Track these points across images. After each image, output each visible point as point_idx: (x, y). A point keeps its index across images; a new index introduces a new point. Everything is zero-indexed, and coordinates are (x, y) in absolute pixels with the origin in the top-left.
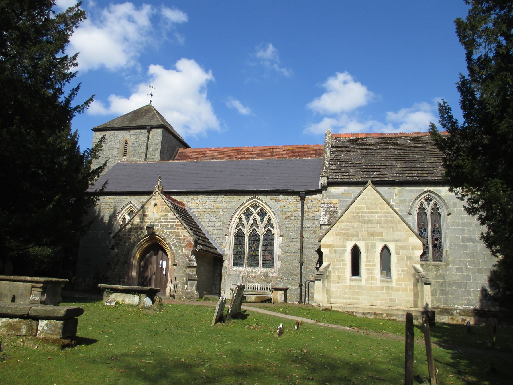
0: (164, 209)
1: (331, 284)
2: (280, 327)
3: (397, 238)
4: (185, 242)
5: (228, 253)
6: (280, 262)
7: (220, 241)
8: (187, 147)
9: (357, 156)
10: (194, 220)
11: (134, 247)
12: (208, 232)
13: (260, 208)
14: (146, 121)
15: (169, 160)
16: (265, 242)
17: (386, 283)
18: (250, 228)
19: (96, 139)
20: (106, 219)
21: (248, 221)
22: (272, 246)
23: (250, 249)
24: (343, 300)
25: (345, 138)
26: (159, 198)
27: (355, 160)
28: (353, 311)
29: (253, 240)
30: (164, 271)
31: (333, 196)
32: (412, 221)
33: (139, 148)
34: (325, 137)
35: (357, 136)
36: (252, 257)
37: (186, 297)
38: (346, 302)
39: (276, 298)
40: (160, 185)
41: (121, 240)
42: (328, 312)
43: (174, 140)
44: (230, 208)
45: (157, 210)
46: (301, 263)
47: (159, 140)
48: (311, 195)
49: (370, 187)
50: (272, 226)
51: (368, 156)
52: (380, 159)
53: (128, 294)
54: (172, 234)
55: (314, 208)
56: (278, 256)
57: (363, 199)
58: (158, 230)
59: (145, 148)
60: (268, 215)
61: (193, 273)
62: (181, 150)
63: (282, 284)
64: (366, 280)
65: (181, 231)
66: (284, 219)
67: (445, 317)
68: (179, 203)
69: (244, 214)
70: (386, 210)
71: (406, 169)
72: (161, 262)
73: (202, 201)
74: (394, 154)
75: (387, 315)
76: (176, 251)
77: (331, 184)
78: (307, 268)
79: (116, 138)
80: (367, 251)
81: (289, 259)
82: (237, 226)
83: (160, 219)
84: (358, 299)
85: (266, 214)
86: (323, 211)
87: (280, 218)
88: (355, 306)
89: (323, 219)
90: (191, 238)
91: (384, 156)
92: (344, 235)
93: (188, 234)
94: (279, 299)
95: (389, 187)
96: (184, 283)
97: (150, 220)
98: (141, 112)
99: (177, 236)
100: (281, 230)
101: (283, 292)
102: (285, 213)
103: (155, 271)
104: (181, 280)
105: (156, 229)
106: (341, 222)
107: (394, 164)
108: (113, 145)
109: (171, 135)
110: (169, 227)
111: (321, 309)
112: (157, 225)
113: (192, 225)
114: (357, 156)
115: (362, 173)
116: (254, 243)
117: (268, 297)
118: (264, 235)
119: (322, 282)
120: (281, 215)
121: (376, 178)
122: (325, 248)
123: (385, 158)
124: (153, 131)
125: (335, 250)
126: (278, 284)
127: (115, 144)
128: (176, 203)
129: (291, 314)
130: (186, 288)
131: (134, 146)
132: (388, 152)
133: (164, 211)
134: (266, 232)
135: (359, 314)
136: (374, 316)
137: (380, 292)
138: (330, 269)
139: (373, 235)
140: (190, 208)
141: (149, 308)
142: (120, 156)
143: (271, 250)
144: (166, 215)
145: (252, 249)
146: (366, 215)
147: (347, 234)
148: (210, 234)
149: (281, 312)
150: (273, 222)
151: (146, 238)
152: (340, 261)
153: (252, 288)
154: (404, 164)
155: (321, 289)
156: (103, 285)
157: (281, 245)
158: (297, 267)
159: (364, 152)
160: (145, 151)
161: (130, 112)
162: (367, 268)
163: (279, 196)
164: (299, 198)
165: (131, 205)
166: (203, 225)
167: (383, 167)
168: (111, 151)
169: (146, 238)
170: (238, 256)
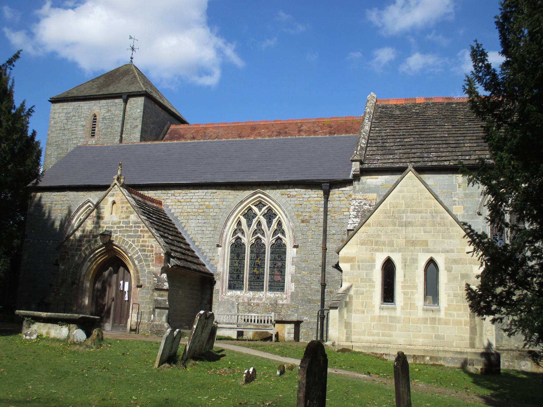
0: (125, 209)
1: (353, 315)
2: (248, 372)
3: (448, 248)
4: (152, 254)
5: (222, 272)
6: (294, 284)
7: (210, 255)
8: (183, 122)
9: (409, 131)
10: (174, 225)
11: (85, 262)
12: (194, 242)
13: (267, 206)
14: (123, 87)
15: (156, 139)
16: (273, 255)
17: (431, 313)
18: (253, 236)
19: (55, 113)
20: (57, 224)
21: (249, 226)
22: (283, 260)
23: (253, 265)
24: (383, 338)
25: (395, 105)
26: (118, 193)
27: (405, 137)
28: (382, 352)
29: (256, 253)
30: (126, 295)
31: (369, 188)
32: (482, 224)
33: (112, 125)
34: (366, 104)
35: (412, 102)
36: (254, 277)
37: (152, 332)
38: (373, 340)
39: (283, 334)
40: (121, 175)
41: (67, 252)
42: (346, 354)
43: (163, 113)
44: (225, 207)
45: (116, 210)
46: (324, 286)
47: (139, 112)
48: (338, 188)
49: (410, 175)
50: (283, 233)
51: (425, 130)
52: (442, 135)
53: (55, 325)
54: (136, 244)
55: (342, 206)
56: (290, 276)
57: (400, 192)
58: (117, 238)
59: (120, 124)
60: (277, 217)
61: (164, 298)
62: (173, 127)
63: (296, 315)
64: (403, 308)
65: (147, 239)
66: (300, 222)
67: (527, 362)
68: (152, 200)
69: (245, 215)
70: (433, 208)
71: (477, 149)
72: (121, 282)
73: (187, 197)
74: (462, 127)
75: (431, 358)
76: (140, 267)
77: (365, 172)
78: (331, 292)
79: (81, 111)
80: (405, 266)
81: (306, 280)
82: (235, 233)
83: (120, 222)
84: (390, 336)
85: (275, 215)
86: (353, 211)
87: (294, 221)
88: (386, 345)
89: (352, 222)
90: (162, 250)
91: (447, 130)
92: (372, 245)
93: (157, 243)
94: (286, 336)
95: (449, 175)
96: (150, 311)
97: (106, 224)
98: (118, 74)
99: (142, 246)
100: (295, 238)
101: (292, 326)
102: (301, 213)
103: (114, 295)
104: (146, 308)
105: (114, 236)
106: (369, 225)
107: (461, 142)
108: (77, 121)
109: (157, 106)
110: (132, 234)
111: (336, 350)
112: (116, 230)
113: (169, 232)
114: (409, 131)
115: (413, 155)
116: (257, 258)
117: (267, 332)
118: (271, 246)
119: (339, 311)
120: (295, 217)
121: (432, 161)
122: (345, 262)
123: (449, 132)
124: (132, 101)
125: (359, 266)
126: (290, 315)
127: (79, 119)
128: (148, 200)
129: (290, 357)
130: (152, 319)
131: (105, 122)
132: (455, 124)
133: (125, 212)
134: (275, 241)
135: (391, 358)
136: (412, 360)
137: (422, 326)
138: (352, 292)
139: (413, 243)
140: (170, 207)
141: (81, 344)
142: (86, 137)
143: (282, 268)
144: (128, 217)
145: (254, 265)
146: (404, 215)
147: (377, 243)
148: (197, 244)
149: (275, 353)
150: (285, 227)
151: (101, 249)
152: (365, 282)
153: (246, 320)
154: (475, 141)
155: (338, 321)
156: (22, 312)
157: (295, 260)
158: (318, 291)
159: (420, 125)
160: (120, 130)
161: (102, 75)
162: (404, 292)
163: (293, 190)
164: (321, 193)
165: (90, 204)
166: (187, 232)
167: (444, 147)
168: (74, 130)
169: (101, 249)
170: (235, 276)
